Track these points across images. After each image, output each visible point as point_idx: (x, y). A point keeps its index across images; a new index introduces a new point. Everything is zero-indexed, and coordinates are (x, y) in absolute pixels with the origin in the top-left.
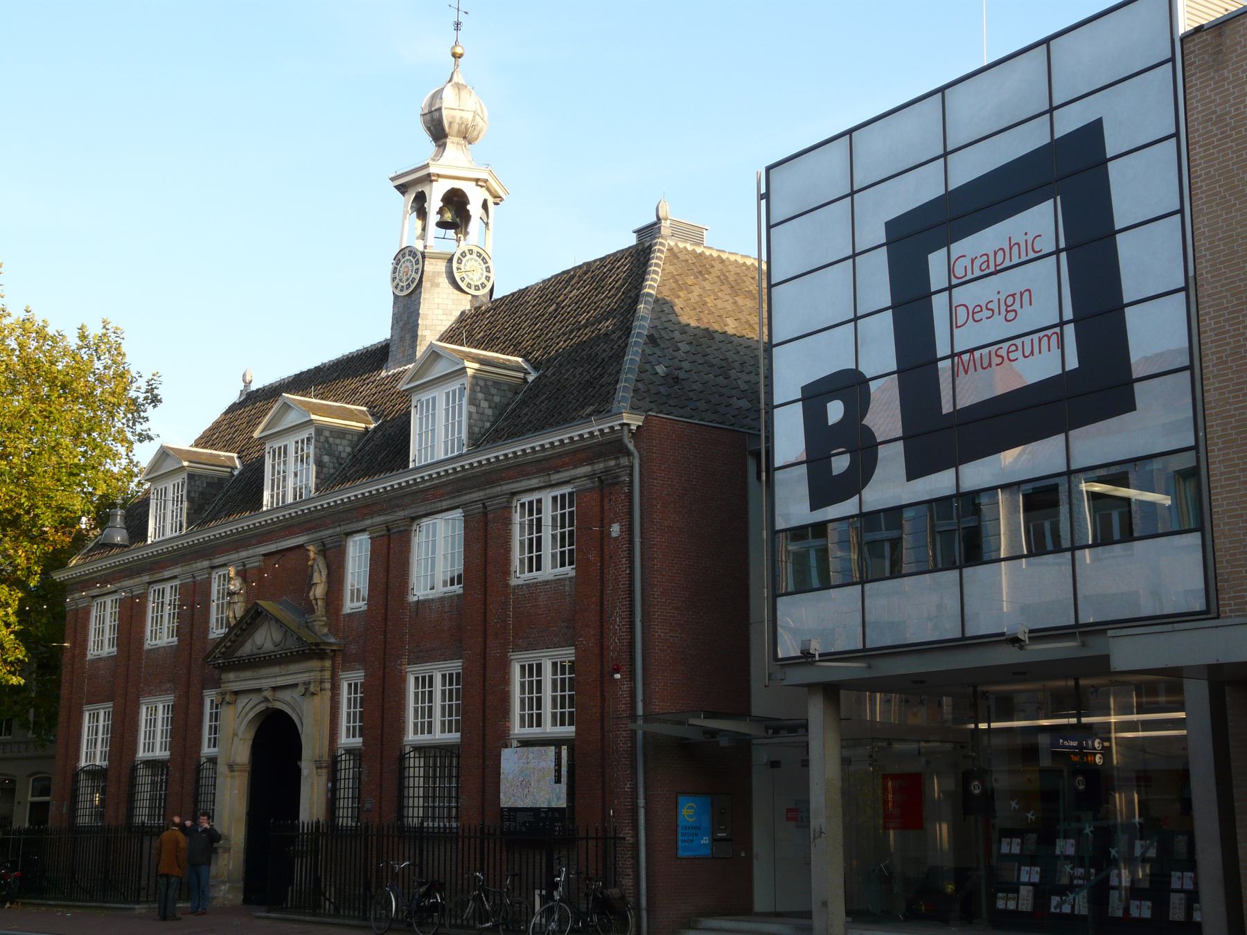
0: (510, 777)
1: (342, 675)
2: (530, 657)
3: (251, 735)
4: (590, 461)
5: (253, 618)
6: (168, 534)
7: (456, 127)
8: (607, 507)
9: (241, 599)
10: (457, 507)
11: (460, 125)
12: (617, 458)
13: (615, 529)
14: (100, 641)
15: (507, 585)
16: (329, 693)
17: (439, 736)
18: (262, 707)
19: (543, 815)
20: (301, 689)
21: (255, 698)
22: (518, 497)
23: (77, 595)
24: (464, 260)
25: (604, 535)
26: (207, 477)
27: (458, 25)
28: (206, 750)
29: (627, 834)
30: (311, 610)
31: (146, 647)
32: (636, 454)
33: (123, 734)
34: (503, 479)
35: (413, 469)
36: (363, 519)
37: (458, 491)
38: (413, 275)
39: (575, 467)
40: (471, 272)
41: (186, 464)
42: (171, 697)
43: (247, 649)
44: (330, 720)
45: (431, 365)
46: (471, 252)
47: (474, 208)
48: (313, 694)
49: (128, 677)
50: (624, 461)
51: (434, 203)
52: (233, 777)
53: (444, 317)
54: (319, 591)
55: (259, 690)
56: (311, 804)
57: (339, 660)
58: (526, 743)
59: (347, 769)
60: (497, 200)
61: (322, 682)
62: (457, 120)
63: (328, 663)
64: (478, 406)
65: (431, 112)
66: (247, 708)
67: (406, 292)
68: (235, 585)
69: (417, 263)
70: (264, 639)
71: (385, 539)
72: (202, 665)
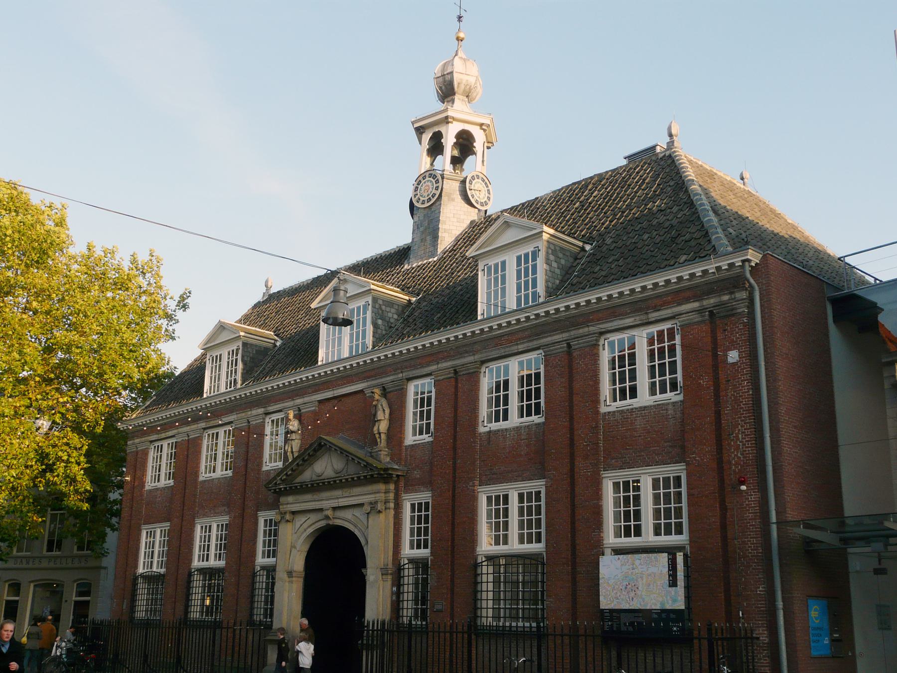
0: (612, 582)
1: (405, 496)
2: (205, 521)
3: (306, 548)
4: (697, 298)
5: (314, 449)
6: (223, 389)
7: (462, 87)
8: (720, 336)
9: (298, 437)
10: (538, 349)
12: (731, 293)
13: (733, 356)
14: (158, 472)
15: (597, 412)
16: (392, 512)
18: (322, 523)
19: (655, 616)
20: (367, 508)
21: (313, 517)
23: (137, 441)
24: (474, 182)
25: (717, 362)
26: (256, 346)
27: (460, 18)
28: (261, 560)
29: (763, 636)
31: (201, 479)
32: (756, 288)
33: (179, 547)
34: (592, 320)
35: (481, 320)
36: (428, 365)
37: (537, 335)
38: (434, 191)
39: (679, 304)
40: (477, 191)
41: (242, 334)
43: (307, 476)
44: (392, 536)
45: (500, 234)
47: (478, 145)
48: (288, 521)
49: (184, 502)
50: (744, 295)
51: (449, 141)
54: (383, 426)
55: (321, 510)
56: (377, 605)
57: (402, 484)
59: (409, 573)
60: (490, 145)
61: (386, 502)
63: (392, 487)
64: (550, 265)
65: (443, 75)
68: (294, 425)
69: (437, 182)
70: (325, 467)
72: (253, 493)
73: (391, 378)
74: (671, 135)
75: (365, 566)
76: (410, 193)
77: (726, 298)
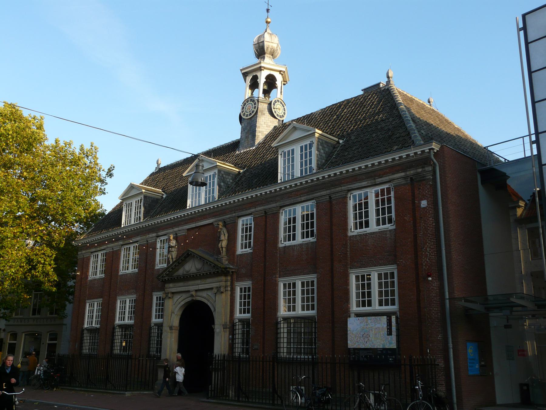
3: (180, 313)
5: (184, 257)
6: (133, 223)
7: (269, 50)
9: (176, 250)
11: (271, 49)
12: (423, 167)
14: (96, 269)
15: (347, 236)
16: (229, 293)
17: (127, 321)
18: (189, 299)
19: (379, 352)
20: (215, 290)
22: (353, 192)
23: (84, 252)
25: (415, 207)
27: (268, 10)
30: (219, 253)
31: (120, 273)
33: (108, 312)
35: (280, 183)
36: (250, 209)
39: (393, 174)
40: (278, 109)
42: (135, 296)
43: (181, 272)
44: (231, 306)
46: (278, 101)
47: (279, 83)
49: (111, 286)
51: (262, 80)
52: (171, 333)
53: (267, 128)
54: (224, 243)
55: (189, 291)
56: (220, 345)
57: (235, 276)
58: (358, 315)
60: (285, 83)
62: (270, 47)
63: (229, 278)
65: (258, 43)
66: (180, 300)
67: (249, 117)
68: (173, 243)
69: (255, 104)
70: (191, 267)
71: (264, 217)
72: (149, 282)
73: (229, 216)
74: (388, 77)
75: (214, 324)
76: (239, 111)
77: (420, 170)
